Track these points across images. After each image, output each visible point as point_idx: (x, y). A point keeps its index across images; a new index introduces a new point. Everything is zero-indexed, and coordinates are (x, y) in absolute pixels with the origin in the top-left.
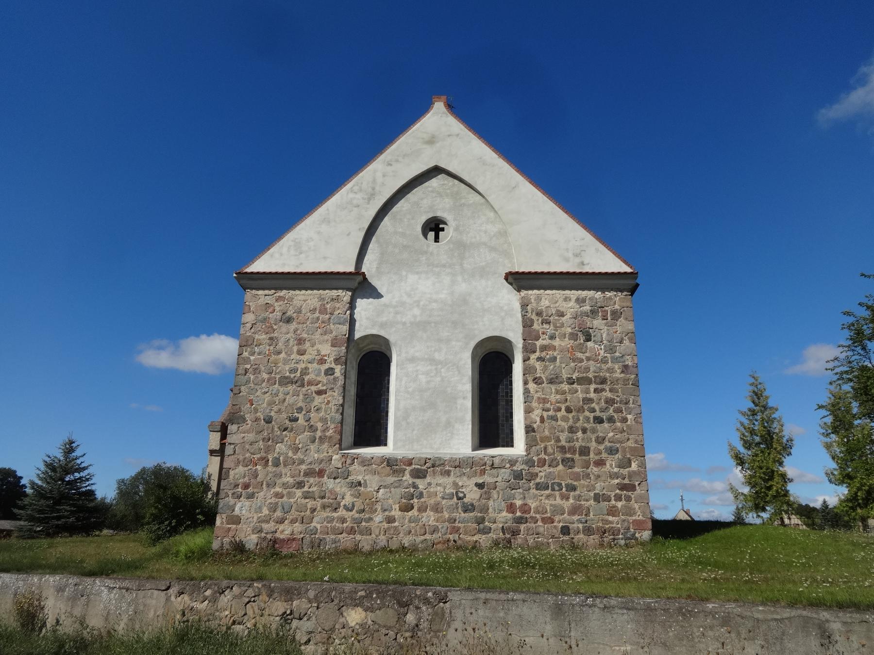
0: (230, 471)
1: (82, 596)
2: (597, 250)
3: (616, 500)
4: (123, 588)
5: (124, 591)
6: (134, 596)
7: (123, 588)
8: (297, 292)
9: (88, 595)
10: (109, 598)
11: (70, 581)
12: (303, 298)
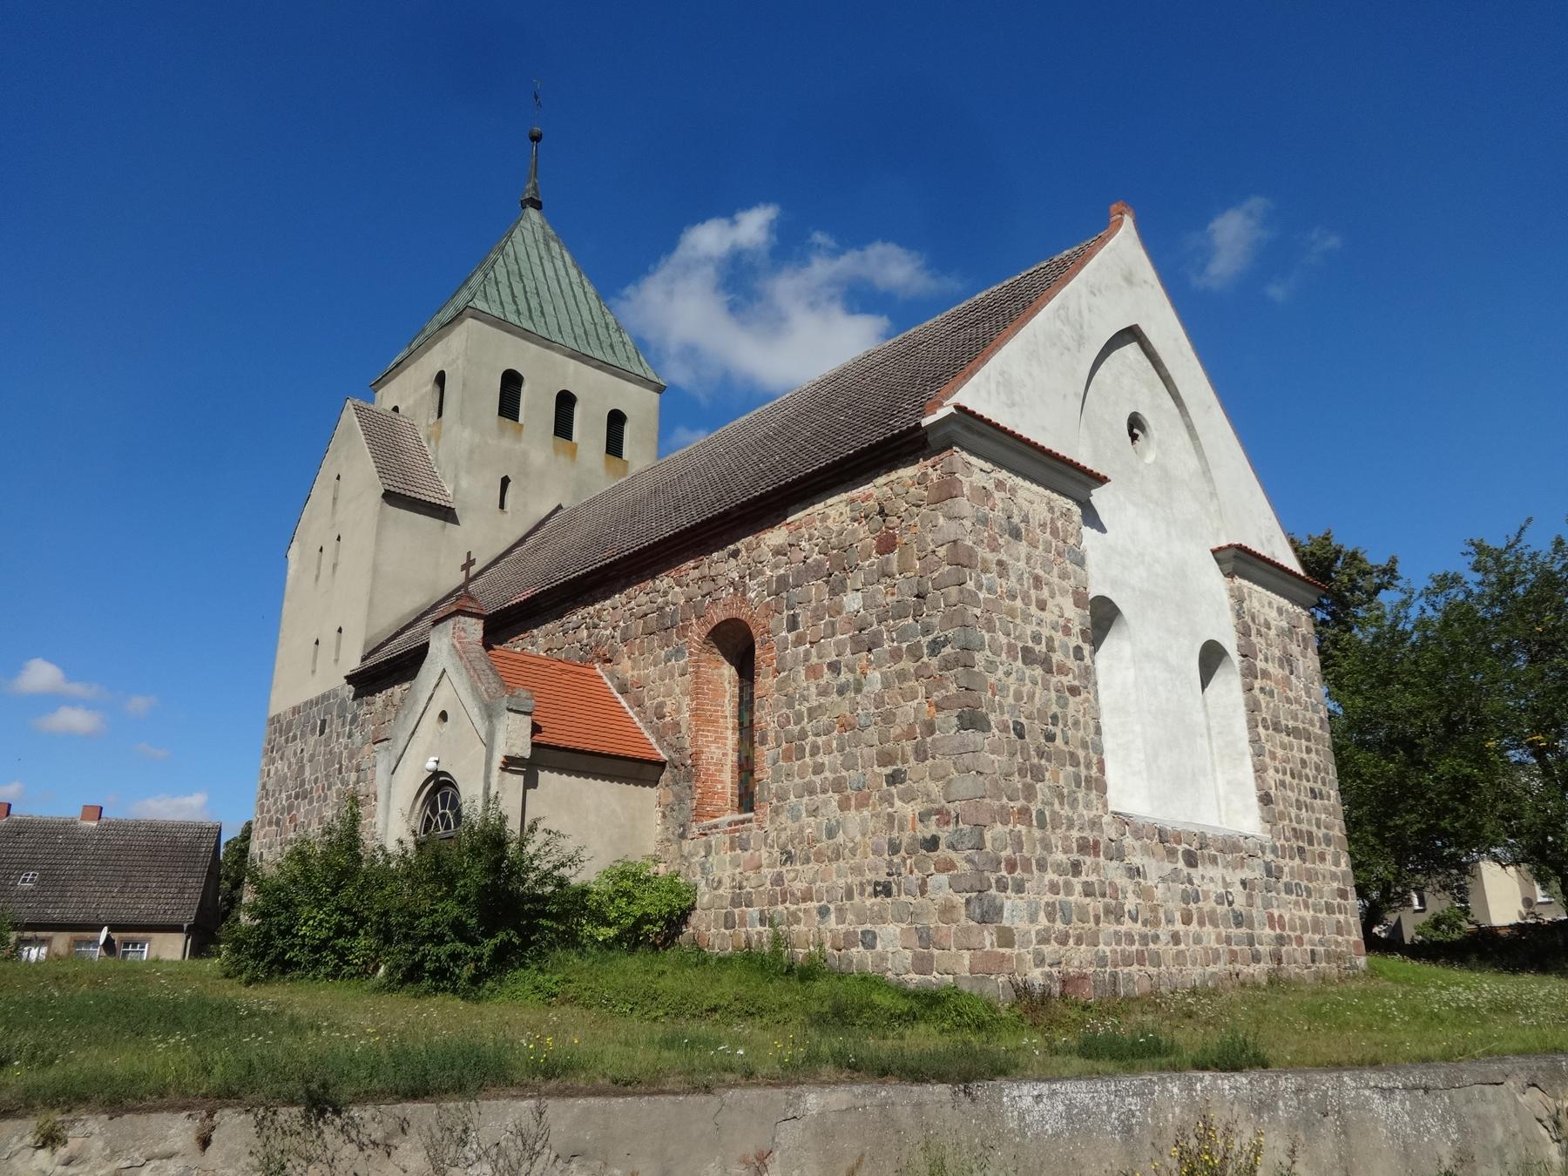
0: (985, 831)
1: (1326, 1115)
2: (1017, 426)
3: (998, 889)
4: (1415, 1088)
5: (1421, 1092)
6: (1447, 1101)
7: (1415, 1088)
8: (1027, 484)
9: (1339, 1112)
10: (1393, 1112)
11: (1282, 1083)
12: (1030, 496)
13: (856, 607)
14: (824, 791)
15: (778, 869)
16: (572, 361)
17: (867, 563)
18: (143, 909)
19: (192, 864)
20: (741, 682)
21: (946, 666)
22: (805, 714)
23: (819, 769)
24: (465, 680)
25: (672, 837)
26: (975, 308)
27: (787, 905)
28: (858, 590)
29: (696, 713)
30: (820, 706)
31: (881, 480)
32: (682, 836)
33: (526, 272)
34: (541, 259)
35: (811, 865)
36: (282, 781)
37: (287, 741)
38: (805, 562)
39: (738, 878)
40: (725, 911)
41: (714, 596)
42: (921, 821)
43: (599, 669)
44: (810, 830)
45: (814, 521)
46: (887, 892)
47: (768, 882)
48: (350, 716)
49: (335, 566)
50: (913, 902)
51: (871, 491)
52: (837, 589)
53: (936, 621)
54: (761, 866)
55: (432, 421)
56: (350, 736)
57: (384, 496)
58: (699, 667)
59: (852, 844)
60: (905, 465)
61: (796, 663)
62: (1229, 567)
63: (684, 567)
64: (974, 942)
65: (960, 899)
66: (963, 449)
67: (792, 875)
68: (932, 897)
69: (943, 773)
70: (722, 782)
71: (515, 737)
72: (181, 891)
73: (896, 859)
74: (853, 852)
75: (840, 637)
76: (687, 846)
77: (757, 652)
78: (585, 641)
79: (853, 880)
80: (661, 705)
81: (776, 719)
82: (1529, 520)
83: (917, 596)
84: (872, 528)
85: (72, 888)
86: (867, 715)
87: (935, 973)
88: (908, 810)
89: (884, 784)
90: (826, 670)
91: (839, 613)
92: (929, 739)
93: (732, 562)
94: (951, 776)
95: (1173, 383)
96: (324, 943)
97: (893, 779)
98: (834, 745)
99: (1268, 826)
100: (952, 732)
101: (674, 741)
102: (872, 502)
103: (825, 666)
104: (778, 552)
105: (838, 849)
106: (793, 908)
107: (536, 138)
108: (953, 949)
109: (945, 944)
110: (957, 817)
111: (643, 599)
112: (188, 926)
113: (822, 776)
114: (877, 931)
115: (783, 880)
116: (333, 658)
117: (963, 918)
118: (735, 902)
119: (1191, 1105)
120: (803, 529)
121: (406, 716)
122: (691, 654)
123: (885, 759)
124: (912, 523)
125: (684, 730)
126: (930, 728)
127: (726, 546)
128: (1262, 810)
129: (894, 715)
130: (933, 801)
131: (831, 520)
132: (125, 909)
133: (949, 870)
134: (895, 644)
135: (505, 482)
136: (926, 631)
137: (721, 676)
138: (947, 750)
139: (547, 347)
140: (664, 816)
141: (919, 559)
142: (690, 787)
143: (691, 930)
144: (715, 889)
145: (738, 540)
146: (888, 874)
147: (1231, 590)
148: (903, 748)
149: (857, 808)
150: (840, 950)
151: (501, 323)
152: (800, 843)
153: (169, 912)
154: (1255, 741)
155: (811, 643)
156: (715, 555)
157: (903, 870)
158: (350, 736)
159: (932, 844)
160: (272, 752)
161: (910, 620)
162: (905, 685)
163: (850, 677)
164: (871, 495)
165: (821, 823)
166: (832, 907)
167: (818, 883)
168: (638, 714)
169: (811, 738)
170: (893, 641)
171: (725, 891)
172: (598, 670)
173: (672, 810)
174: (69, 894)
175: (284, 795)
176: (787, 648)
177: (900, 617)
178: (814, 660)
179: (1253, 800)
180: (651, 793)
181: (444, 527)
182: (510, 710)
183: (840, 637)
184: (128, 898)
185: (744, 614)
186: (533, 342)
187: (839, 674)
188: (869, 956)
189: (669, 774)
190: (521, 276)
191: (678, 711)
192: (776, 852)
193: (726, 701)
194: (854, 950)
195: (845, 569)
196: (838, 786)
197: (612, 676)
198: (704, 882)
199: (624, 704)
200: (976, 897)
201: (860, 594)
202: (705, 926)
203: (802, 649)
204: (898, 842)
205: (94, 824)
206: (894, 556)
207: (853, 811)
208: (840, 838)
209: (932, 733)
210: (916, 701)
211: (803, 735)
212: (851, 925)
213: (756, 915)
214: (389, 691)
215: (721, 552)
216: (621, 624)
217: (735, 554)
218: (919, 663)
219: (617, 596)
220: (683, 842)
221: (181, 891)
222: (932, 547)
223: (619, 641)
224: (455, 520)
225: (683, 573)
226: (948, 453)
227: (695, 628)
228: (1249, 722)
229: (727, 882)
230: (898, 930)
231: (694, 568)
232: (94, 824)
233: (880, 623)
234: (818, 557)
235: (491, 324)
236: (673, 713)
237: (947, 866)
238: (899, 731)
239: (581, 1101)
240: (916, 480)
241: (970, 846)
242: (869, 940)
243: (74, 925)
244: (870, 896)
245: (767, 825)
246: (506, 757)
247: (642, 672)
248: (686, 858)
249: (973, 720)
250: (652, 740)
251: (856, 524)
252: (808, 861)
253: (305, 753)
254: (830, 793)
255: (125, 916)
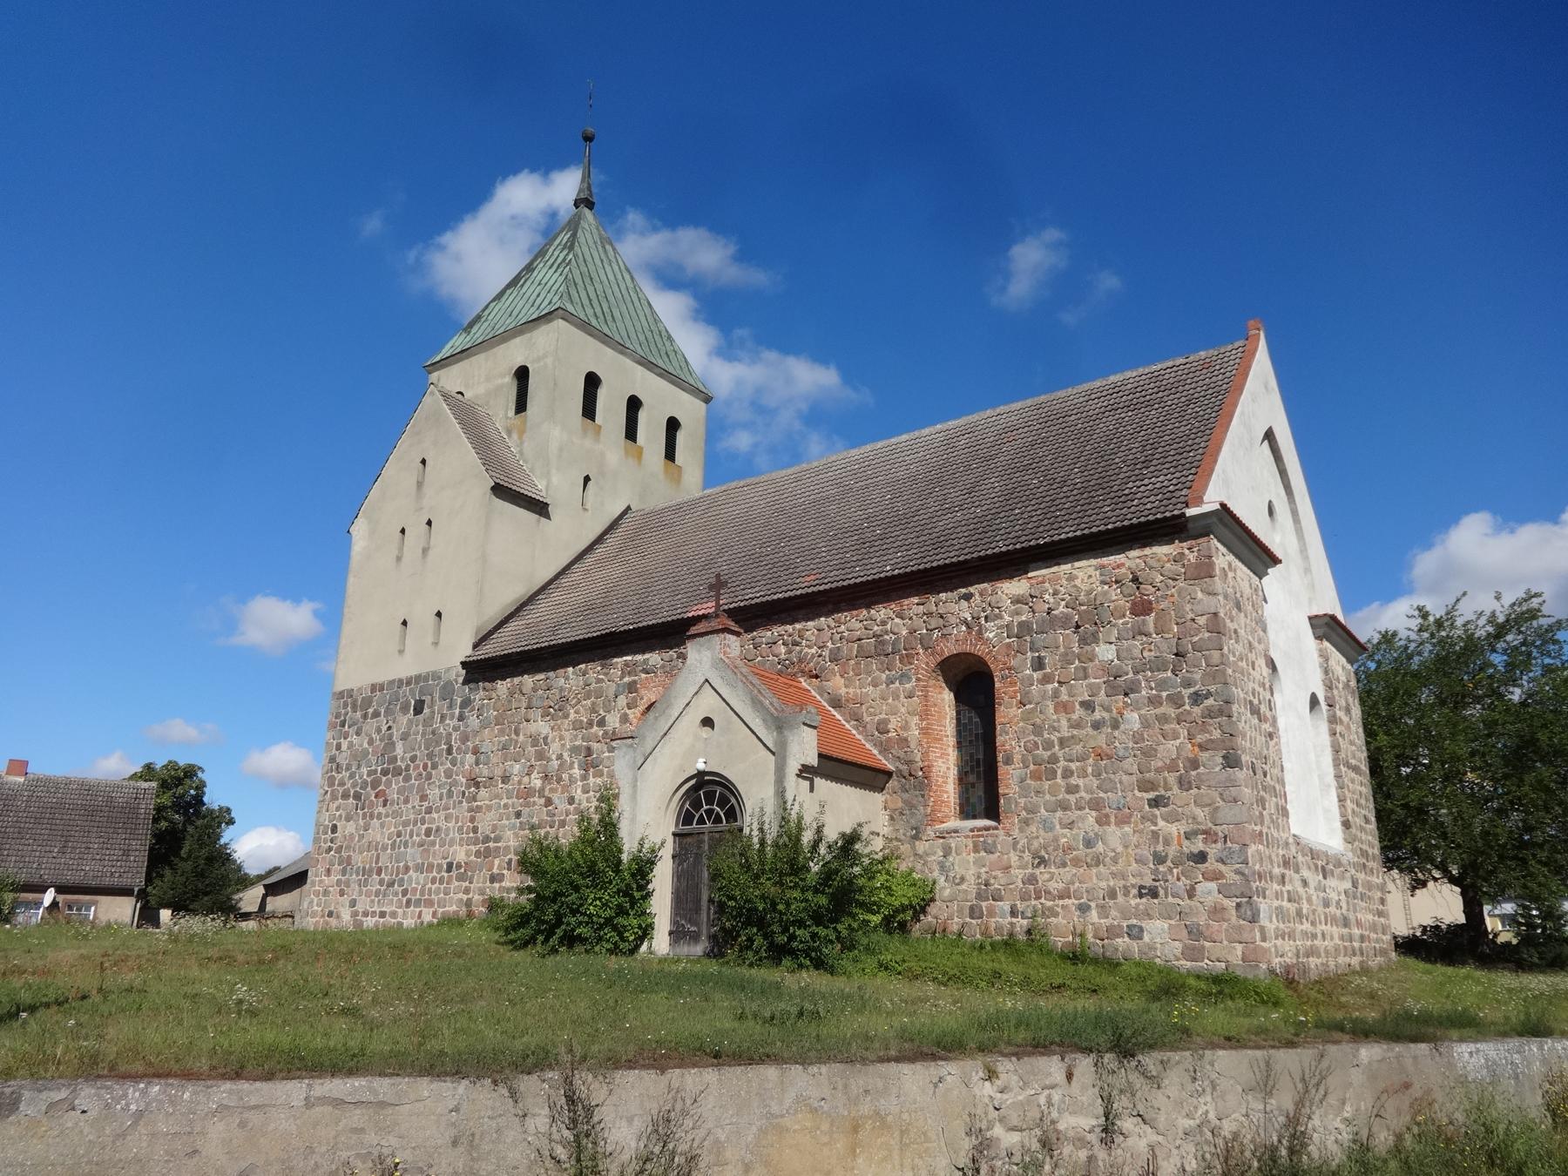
13: (1111, 658)
14: (1081, 809)
15: (1030, 870)
16: (640, 367)
17: (1121, 621)
18: (89, 871)
19: (133, 826)
20: (957, 706)
21: (1210, 714)
22: (1056, 742)
23: (1072, 790)
24: (741, 693)
25: (903, 837)
26: (1116, 389)
27: (1043, 900)
28: (1111, 643)
29: (925, 731)
30: (1073, 737)
31: (1134, 553)
32: (916, 837)
33: (594, 275)
34: (602, 261)
35: (1067, 869)
36: (359, 757)
37: (365, 716)
38: (1048, 613)
39: (984, 876)
40: (969, 904)
41: (945, 632)
42: (1187, 838)
43: (804, 683)
44: (1066, 840)
45: (1060, 578)
46: (1154, 894)
47: (1020, 881)
48: (459, 700)
49: (425, 551)
50: (1181, 903)
51: (1123, 561)
52: (1088, 640)
53: (1197, 676)
54: (1011, 867)
55: (511, 413)
56: (461, 718)
57: (493, 488)
58: (928, 691)
59: (1113, 854)
60: (1160, 543)
61: (1044, 697)
62: (1320, 632)
63: (906, 602)
64: (1246, 936)
65: (1230, 904)
66: (1216, 537)
67: (1047, 876)
68: (1201, 900)
69: (1210, 802)
70: (947, 792)
71: (805, 747)
72: (126, 853)
73: (1161, 868)
74: (1115, 860)
75: (1093, 681)
76: (921, 847)
77: (997, 685)
78: (783, 656)
79: (1117, 884)
80: (886, 722)
81: (1022, 744)
82: (1465, 594)
83: (1176, 655)
84: (1126, 593)
85: (8, 846)
86: (1126, 749)
87: (1206, 961)
88: (1173, 829)
89: (1147, 807)
90: (1078, 707)
91: (1091, 660)
92: (1193, 773)
93: (964, 604)
94: (1217, 805)
95: (1287, 475)
96: (609, 921)
97: (1155, 803)
98: (1090, 770)
99: (1350, 846)
100: (1217, 769)
101: (901, 754)
102: (1123, 570)
103: (1077, 704)
104: (1017, 600)
105: (1098, 857)
106: (1050, 904)
107: (588, 138)
108: (1225, 942)
109: (1218, 939)
110: (1225, 837)
111: (855, 624)
112: (139, 890)
113: (1077, 796)
114: (1143, 925)
115: (1037, 881)
116: (430, 639)
117: (1234, 919)
118: (979, 896)
119: (1544, 1061)
120: (1047, 585)
121: (656, 718)
122: (918, 680)
123: (1145, 786)
124: (1169, 593)
125: (913, 745)
126: (1194, 764)
127: (956, 588)
128: (1344, 833)
129: (1156, 750)
130: (1198, 823)
131: (1079, 580)
132: (68, 870)
133: (1217, 879)
134: (1154, 692)
135: (587, 479)
136: (1188, 684)
137: (943, 700)
138: (1213, 783)
139: (622, 353)
140: (892, 818)
141: (1177, 624)
142: (923, 796)
143: (930, 918)
144: (958, 884)
145: (971, 585)
146: (1154, 880)
147: (1320, 650)
148: (1165, 779)
149: (1117, 824)
150: (1103, 940)
151: (585, 326)
152: (1054, 850)
153: (117, 875)
154: (1338, 777)
155: (1059, 682)
156: (943, 596)
157: (1170, 877)
158: (461, 718)
159: (1201, 857)
160: (344, 726)
161: (1169, 674)
162: (1166, 727)
163: (1106, 715)
164: (1123, 565)
165: (1077, 835)
166: (1093, 905)
167: (1077, 884)
168: (856, 728)
169: (1062, 763)
170: (1152, 689)
171: (970, 887)
172: (804, 684)
173: (901, 814)
174: (6, 853)
175: (364, 770)
176: (1033, 685)
177: (1159, 670)
178: (1064, 697)
179: (1338, 825)
180: (878, 798)
181: (539, 521)
182: (805, 724)
183: (1093, 681)
184: (71, 859)
185: (980, 650)
186: (609, 347)
187: (1093, 712)
188: (1135, 946)
189: (896, 783)
190: (591, 279)
191: (906, 727)
192: (1027, 856)
193: (948, 721)
194: (1119, 940)
195: (1096, 624)
196: (1096, 805)
197: (821, 691)
198: (943, 879)
199: (838, 717)
200: (1247, 902)
201: (1113, 646)
202: (947, 912)
203: (1050, 687)
204: (1163, 854)
205: (21, 780)
206: (1151, 619)
207: (1113, 827)
208: (1100, 847)
209: (1196, 768)
210: (1178, 741)
211: (1054, 759)
212: (1114, 918)
213: (1007, 909)
214: (517, 680)
215: (949, 593)
216: (829, 644)
217: (968, 597)
218: (1181, 710)
219: (823, 619)
220: (917, 843)
221: (126, 853)
222: (1191, 615)
223: (827, 659)
224: (547, 516)
225: (905, 607)
226: (1206, 539)
227: (922, 657)
228: (1334, 760)
229: (971, 879)
230: (1166, 926)
231: (917, 604)
232: (21, 780)
233: (1136, 672)
234: (1065, 610)
235: (576, 326)
236: (899, 730)
237: (1215, 876)
238: (1160, 764)
239: (1249, 1052)
240: (1171, 557)
241: (1239, 861)
242: (1135, 933)
243: (67, 887)
244: (1134, 897)
245: (1016, 833)
246: (803, 765)
247: (859, 691)
248: (921, 857)
249: (1231, 761)
250: (875, 752)
251: (1106, 587)
252: (1064, 865)
253: (394, 730)
254: (1087, 810)
255: (70, 878)
